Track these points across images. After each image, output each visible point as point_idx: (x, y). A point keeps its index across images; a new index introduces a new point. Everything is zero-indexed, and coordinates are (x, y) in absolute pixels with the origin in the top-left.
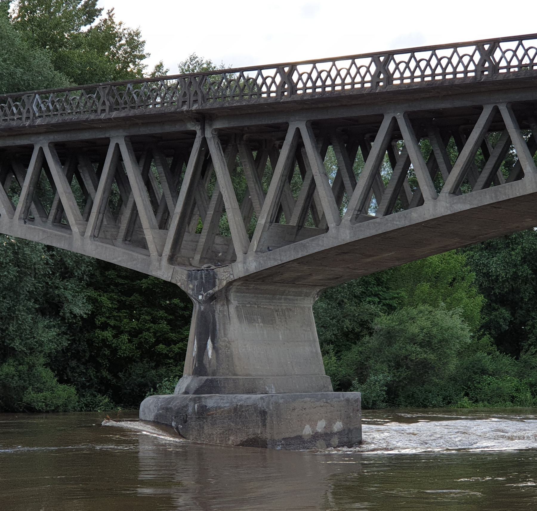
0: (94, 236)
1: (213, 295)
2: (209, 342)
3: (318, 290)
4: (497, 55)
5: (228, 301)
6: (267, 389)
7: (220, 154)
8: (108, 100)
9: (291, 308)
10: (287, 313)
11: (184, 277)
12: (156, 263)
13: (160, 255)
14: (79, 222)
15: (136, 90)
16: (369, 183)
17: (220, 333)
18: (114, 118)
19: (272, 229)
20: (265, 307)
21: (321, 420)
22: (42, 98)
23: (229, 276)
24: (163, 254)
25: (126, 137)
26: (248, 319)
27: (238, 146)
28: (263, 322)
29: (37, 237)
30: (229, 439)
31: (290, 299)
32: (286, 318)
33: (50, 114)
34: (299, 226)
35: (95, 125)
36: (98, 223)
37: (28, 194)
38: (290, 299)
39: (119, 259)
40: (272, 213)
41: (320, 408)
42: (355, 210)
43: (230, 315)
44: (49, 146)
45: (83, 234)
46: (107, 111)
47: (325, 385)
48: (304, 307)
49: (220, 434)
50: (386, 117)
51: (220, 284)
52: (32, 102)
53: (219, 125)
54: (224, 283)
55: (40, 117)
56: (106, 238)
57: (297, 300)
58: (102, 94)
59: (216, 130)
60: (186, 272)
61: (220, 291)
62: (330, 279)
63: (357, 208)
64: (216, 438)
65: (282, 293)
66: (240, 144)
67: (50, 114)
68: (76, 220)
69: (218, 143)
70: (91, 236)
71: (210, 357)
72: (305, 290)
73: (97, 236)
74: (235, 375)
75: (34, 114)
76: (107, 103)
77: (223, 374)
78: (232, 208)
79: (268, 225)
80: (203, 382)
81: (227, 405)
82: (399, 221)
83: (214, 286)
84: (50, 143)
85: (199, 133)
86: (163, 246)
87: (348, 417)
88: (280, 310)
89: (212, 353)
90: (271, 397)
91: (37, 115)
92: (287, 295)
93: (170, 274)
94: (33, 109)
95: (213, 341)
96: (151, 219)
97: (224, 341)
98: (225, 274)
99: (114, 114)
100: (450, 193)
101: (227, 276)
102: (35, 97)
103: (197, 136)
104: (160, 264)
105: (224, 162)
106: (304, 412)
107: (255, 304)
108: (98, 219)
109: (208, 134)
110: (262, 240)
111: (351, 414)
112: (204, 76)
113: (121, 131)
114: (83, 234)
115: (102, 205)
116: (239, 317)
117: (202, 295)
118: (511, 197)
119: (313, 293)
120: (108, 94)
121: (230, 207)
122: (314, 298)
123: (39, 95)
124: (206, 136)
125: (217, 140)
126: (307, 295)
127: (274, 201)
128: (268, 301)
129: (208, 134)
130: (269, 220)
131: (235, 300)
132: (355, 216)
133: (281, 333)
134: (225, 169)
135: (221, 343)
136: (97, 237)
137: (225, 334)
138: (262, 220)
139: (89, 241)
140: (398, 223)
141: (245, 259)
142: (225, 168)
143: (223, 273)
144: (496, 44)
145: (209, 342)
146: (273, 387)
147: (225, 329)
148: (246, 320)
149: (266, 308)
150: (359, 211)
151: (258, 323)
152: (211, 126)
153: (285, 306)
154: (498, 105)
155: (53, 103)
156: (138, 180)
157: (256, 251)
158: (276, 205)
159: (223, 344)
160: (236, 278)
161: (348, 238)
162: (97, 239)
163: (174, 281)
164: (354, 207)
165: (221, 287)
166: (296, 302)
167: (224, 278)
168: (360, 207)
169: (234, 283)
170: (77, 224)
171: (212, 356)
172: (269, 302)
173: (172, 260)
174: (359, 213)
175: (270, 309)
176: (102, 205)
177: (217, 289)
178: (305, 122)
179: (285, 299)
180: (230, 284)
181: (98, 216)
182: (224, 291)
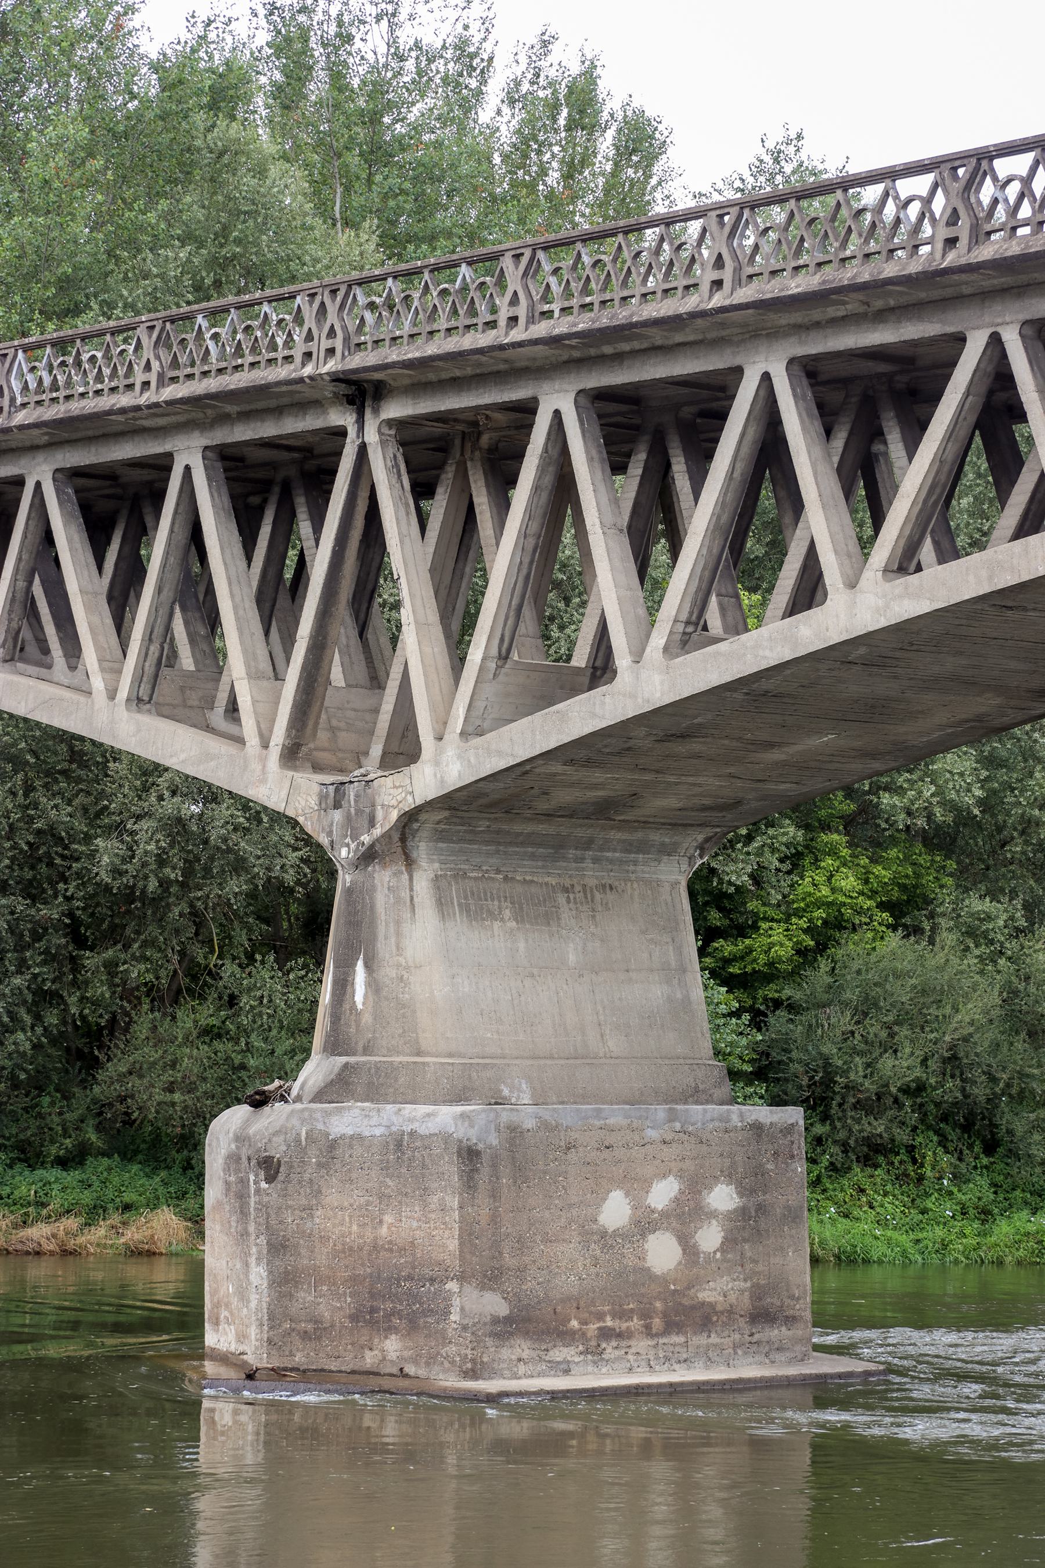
0: (139, 700)
1: (372, 846)
2: (360, 966)
3: (700, 838)
4: (987, 192)
5: (410, 862)
6: (506, 1092)
7: (398, 485)
8: (158, 357)
9: (617, 883)
10: (598, 896)
11: (313, 802)
12: (255, 766)
13: (265, 746)
14: (110, 664)
15: (213, 331)
16: (710, 549)
17: (384, 948)
18: (166, 402)
19: (507, 675)
20: (528, 878)
21: (664, 1176)
22: (28, 360)
23: (405, 798)
24: (272, 744)
25: (206, 448)
26: (468, 911)
27: (469, 464)
28: (519, 917)
29: (23, 704)
30: (381, 1222)
31: (611, 861)
32: (593, 910)
33: (44, 397)
34: (594, 668)
35: (146, 423)
36: (147, 668)
37: (13, 600)
38: (611, 861)
39: (182, 757)
40: (503, 636)
41: (664, 1147)
42: (676, 621)
43: (416, 900)
44: (54, 480)
45: (112, 695)
46: (153, 384)
47: (701, 1087)
48: (658, 880)
49: (360, 1207)
50: (747, 373)
51: (385, 818)
52: (9, 371)
53: (395, 409)
54: (394, 815)
55: (24, 405)
56: (185, 706)
57: (635, 863)
58: (145, 341)
59: (390, 423)
60: (316, 788)
61: (387, 836)
62: (705, 808)
63: (684, 616)
64: (350, 1217)
65: (588, 844)
66: (472, 460)
67: (44, 397)
68: (100, 661)
69: (395, 456)
70: (128, 700)
71: (360, 1006)
72: (656, 837)
73: (146, 698)
74: (419, 1054)
75: (13, 400)
76: (155, 365)
77: (389, 1050)
78: (416, 622)
79: (492, 665)
80: (336, 1070)
81: (378, 1132)
82: (771, 650)
83: (372, 823)
84: (57, 471)
85: (352, 432)
86: (273, 721)
87: (759, 1172)
88: (578, 888)
89: (366, 996)
90: (318, 1115)
91: (19, 401)
92: (601, 849)
93: (284, 794)
94: (10, 388)
95: (367, 966)
96: (254, 654)
97: (398, 966)
98: (395, 792)
99: (169, 393)
100: (886, 570)
101: (399, 798)
102: (15, 356)
103: (348, 440)
104: (264, 767)
105: (407, 505)
106: (606, 1154)
107: (498, 872)
108: (146, 655)
109: (371, 436)
110: (480, 704)
111: (770, 1166)
112: (350, 286)
113: (196, 434)
114: (112, 695)
115: (155, 620)
116: (442, 904)
117: (348, 845)
118: (1025, 577)
119: (686, 845)
120: (157, 343)
121: (411, 619)
122: (691, 859)
123: (24, 351)
124: (366, 440)
125: (392, 449)
126: (667, 851)
127: (506, 602)
128: (540, 863)
129: (371, 436)
130: (494, 651)
131: (432, 861)
132: (678, 637)
133: (576, 949)
134: (409, 524)
135: (387, 972)
136: (149, 702)
137: (398, 948)
138: (476, 654)
139: (125, 713)
140: (767, 653)
141: (439, 753)
142: (408, 519)
143: (392, 791)
144: (985, 164)
145: (360, 966)
146: (524, 1086)
147: (398, 934)
148: (461, 911)
149: (532, 881)
150: (688, 623)
151: (502, 920)
152: (376, 411)
153: (597, 878)
154: (999, 329)
155: (50, 368)
156: (228, 556)
157: (463, 734)
158: (512, 613)
159: (393, 973)
160: (419, 802)
161: (658, 695)
162: (148, 706)
163: (290, 813)
164: (674, 613)
165: (387, 827)
166: (632, 868)
167: (394, 802)
168: (691, 613)
169: (423, 817)
170: (103, 670)
171: (364, 1004)
172: (543, 867)
173: (292, 755)
174: (690, 629)
175: (547, 884)
176: (155, 620)
177: (378, 832)
178: (573, 395)
179: (596, 860)
180: (410, 819)
181: (148, 649)
182: (396, 836)
